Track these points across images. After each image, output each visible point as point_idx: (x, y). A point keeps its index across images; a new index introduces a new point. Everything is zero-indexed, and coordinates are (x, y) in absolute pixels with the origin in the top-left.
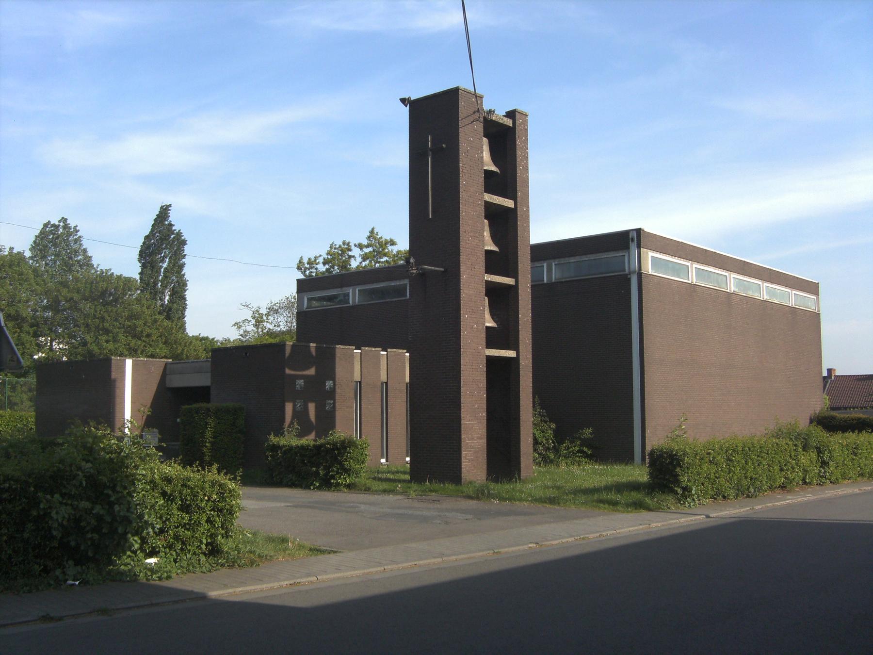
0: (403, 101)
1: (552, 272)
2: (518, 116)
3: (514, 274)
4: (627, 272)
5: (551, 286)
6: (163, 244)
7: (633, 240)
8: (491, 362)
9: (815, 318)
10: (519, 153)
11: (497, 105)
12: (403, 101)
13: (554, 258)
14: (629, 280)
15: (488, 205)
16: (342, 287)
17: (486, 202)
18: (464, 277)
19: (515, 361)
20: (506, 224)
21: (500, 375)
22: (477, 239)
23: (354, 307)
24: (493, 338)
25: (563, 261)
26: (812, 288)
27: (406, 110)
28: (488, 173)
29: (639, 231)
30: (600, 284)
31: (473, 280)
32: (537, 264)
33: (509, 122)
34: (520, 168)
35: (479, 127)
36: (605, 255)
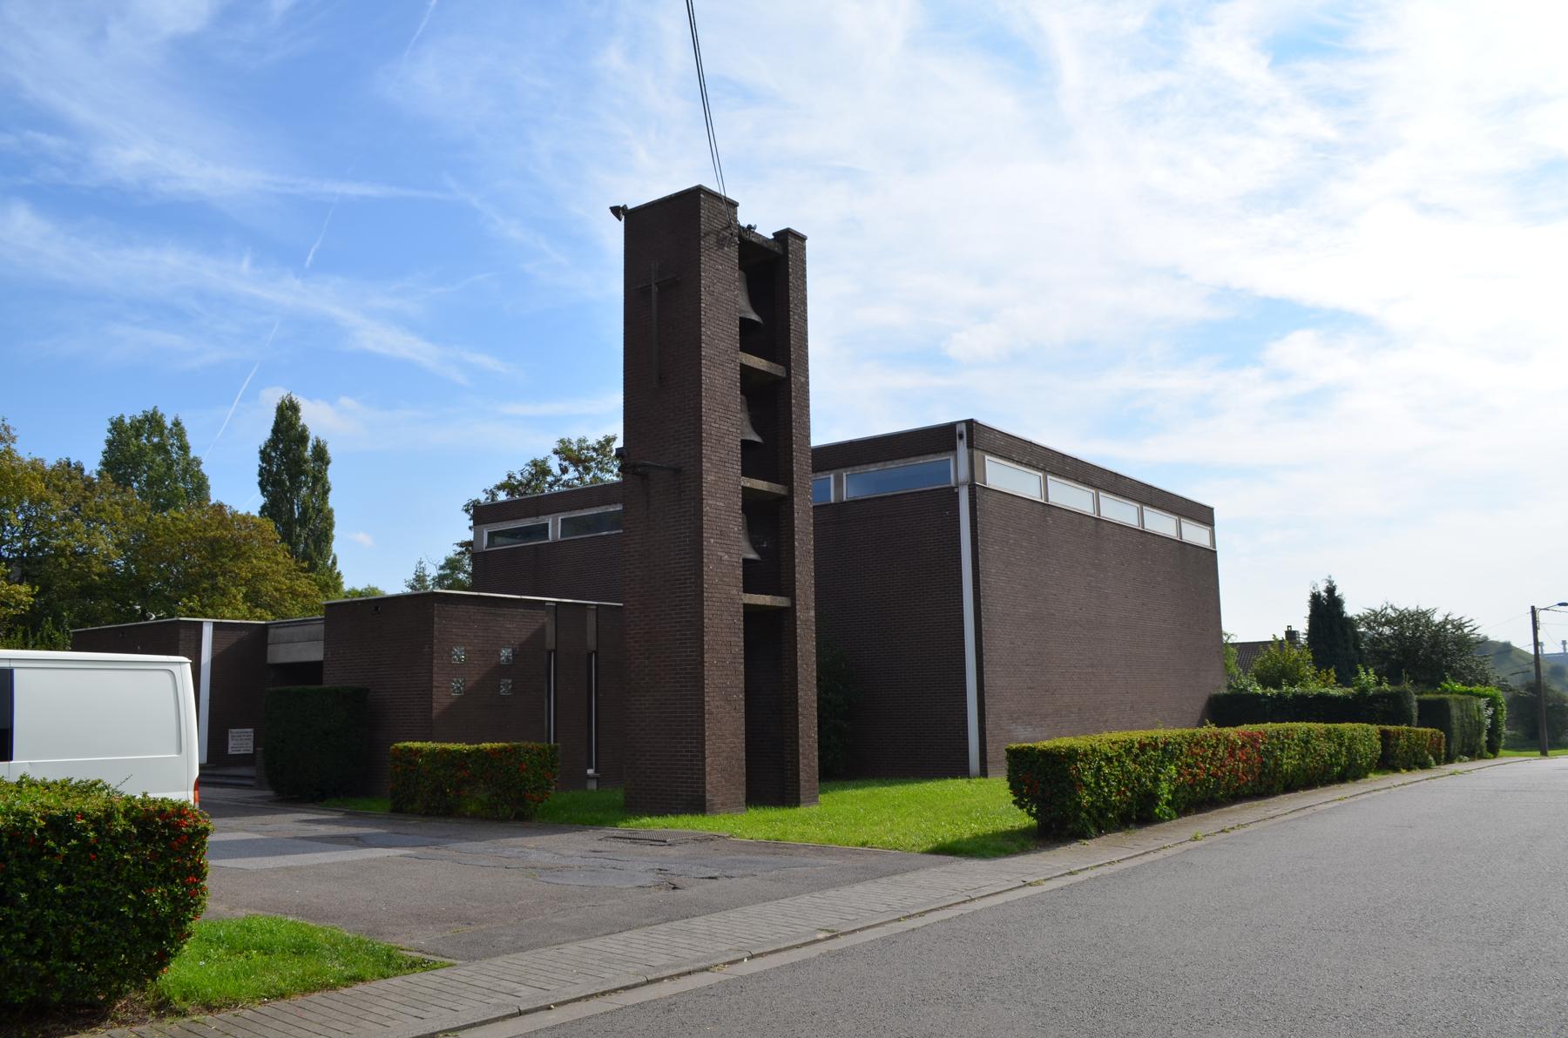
0: (616, 211)
1: (845, 487)
2: (791, 240)
3: (791, 594)
4: (953, 484)
5: (841, 506)
6: (292, 461)
7: (961, 437)
8: (750, 612)
9: (1206, 560)
10: (792, 294)
11: (761, 216)
12: (616, 211)
13: (845, 465)
14: (957, 494)
15: (745, 369)
16: (537, 515)
17: (742, 365)
18: (709, 478)
19: (791, 611)
20: (775, 397)
21: (766, 635)
22: (725, 424)
23: (555, 544)
24: (753, 577)
25: (858, 469)
26: (1204, 515)
27: (618, 227)
28: (745, 324)
29: (970, 423)
30: (923, 488)
31: (723, 484)
32: (821, 476)
33: (777, 249)
34: (794, 318)
35: (733, 252)
36: (921, 461)
